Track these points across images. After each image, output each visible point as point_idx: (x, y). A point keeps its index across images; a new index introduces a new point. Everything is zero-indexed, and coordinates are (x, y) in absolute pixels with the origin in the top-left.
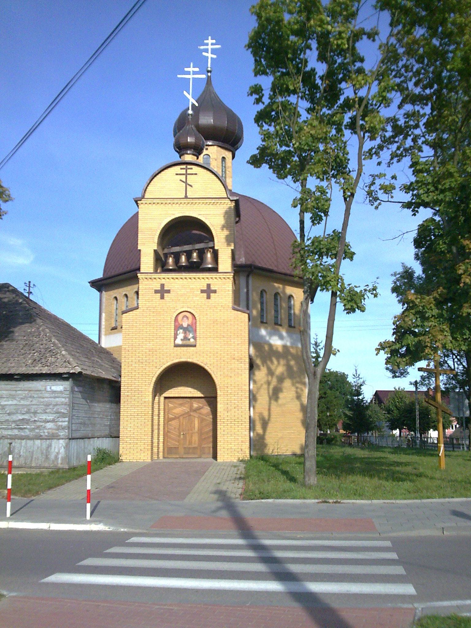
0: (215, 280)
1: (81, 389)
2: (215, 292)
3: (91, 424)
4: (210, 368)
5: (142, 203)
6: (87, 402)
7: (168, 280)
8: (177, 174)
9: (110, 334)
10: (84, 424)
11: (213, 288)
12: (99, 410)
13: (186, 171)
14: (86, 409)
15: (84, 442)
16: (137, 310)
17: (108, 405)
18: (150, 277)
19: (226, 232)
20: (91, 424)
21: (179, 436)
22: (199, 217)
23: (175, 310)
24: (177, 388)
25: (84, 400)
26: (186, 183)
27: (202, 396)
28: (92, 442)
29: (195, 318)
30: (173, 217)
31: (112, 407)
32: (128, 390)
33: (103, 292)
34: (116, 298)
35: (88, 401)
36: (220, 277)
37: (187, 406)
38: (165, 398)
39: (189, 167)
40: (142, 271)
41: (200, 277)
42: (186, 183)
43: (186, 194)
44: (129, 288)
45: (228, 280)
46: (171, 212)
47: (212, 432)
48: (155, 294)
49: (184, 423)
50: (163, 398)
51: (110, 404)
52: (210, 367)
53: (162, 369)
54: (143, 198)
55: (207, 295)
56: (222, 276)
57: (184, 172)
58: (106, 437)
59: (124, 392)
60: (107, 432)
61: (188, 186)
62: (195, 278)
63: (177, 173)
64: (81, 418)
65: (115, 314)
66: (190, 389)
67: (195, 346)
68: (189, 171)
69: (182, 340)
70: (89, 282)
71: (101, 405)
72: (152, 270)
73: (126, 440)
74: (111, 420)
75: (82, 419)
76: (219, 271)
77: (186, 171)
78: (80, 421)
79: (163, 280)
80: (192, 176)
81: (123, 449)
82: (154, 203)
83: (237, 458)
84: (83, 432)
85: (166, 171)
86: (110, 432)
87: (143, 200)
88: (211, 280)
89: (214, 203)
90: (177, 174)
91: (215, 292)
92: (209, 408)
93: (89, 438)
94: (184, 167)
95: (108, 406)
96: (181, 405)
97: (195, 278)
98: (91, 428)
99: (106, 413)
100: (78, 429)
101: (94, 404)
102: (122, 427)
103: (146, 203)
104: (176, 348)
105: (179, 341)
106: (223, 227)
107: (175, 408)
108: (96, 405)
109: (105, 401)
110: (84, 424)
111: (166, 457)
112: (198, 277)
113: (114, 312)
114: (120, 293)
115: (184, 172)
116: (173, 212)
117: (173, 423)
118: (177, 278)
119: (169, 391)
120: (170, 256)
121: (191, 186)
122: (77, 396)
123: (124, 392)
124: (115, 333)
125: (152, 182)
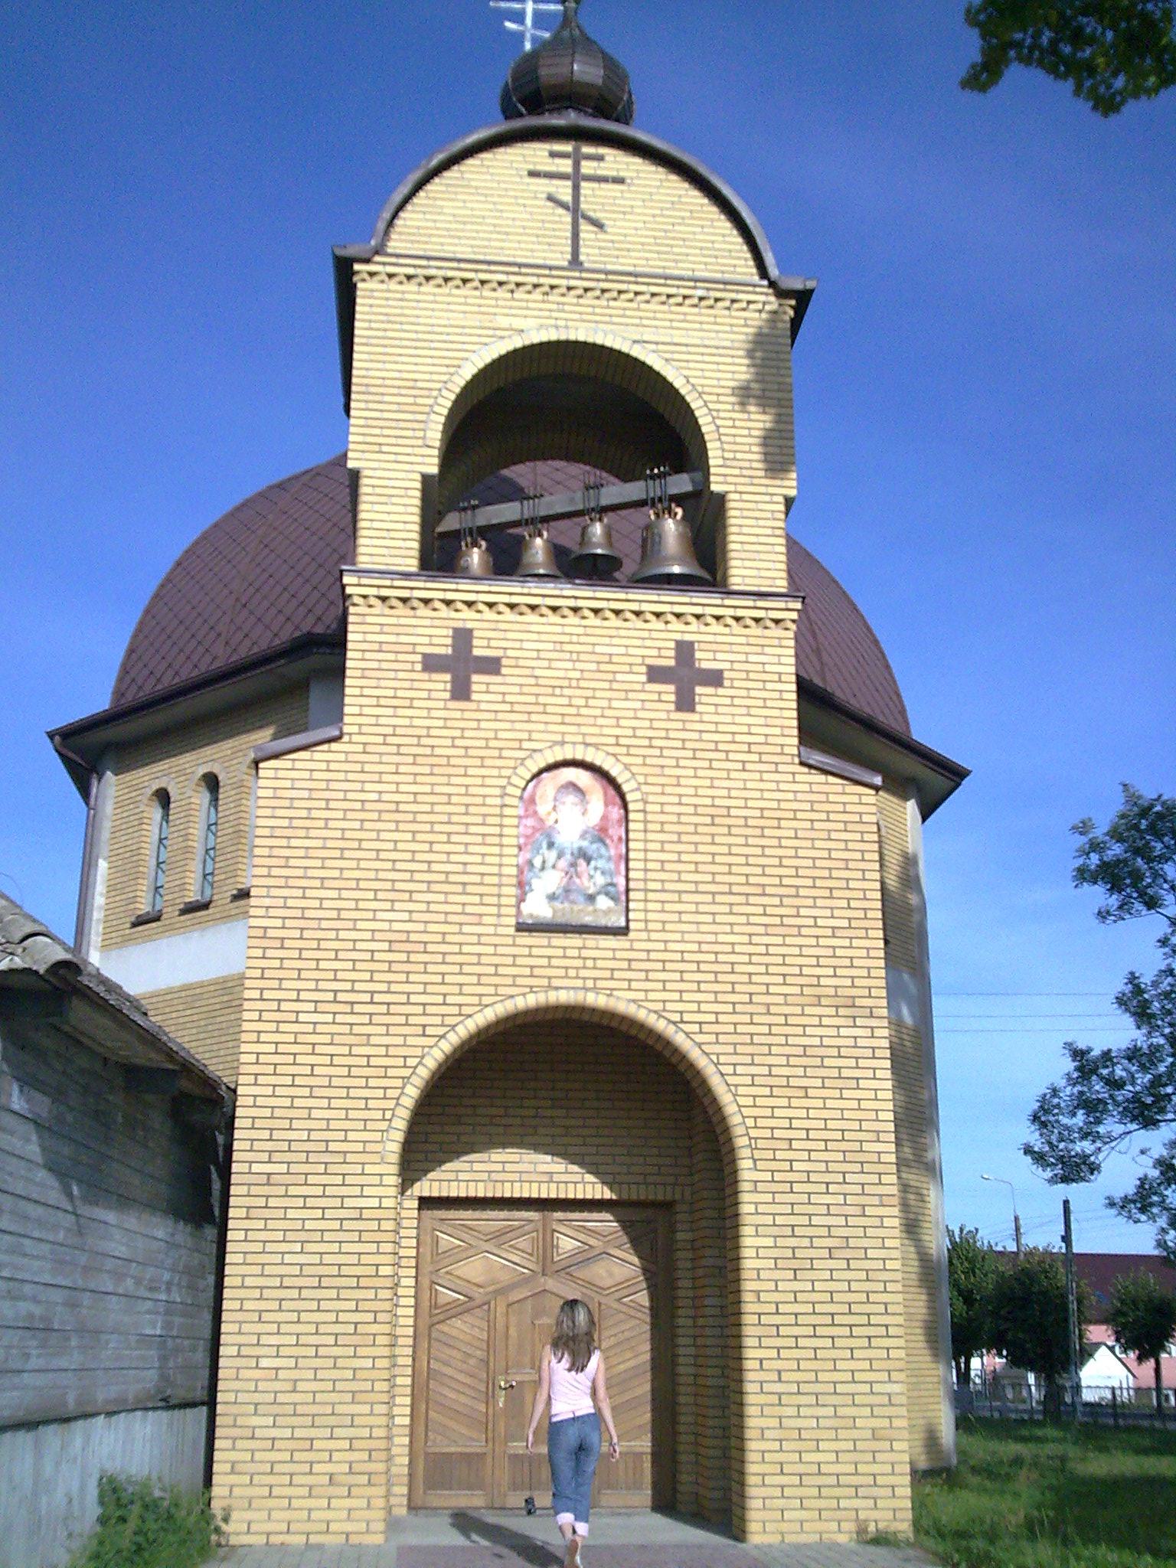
0: (716, 627)
1: (43, 1105)
2: (715, 679)
3: (82, 1330)
4: (699, 1045)
5: (372, 274)
6: (70, 1196)
7: (488, 614)
8: (533, 174)
9: (125, 942)
10: (40, 1329)
11: (705, 660)
12: (122, 1251)
13: (577, 165)
14: (61, 1236)
15: (37, 1444)
16: (334, 746)
17: (161, 1229)
18: (405, 594)
19: (759, 421)
20: (82, 1330)
21: (489, 1398)
22: (636, 352)
23: (522, 754)
24: (483, 1156)
25: (52, 1181)
26: (575, 209)
27: (608, 1194)
28: (78, 1442)
29: (622, 796)
30: (517, 343)
31: (179, 1238)
32: (269, 1146)
33: (109, 773)
34: (163, 798)
35: (75, 1190)
36: (740, 613)
37: (523, 1243)
38: (425, 1203)
39: (587, 149)
40: (363, 561)
41: (645, 607)
42: (575, 209)
43: (575, 252)
44: (227, 747)
45: (776, 632)
46: (504, 322)
47: (648, 1376)
48: (425, 676)
49: (513, 1332)
50: (415, 1204)
51: (170, 1222)
52: (699, 1038)
53: (454, 1039)
54: (377, 253)
55: (678, 693)
56: (747, 608)
57: (565, 166)
58: (143, 1406)
59: (250, 1156)
60: (150, 1378)
61: (584, 226)
62: (617, 612)
63: (531, 167)
64: (28, 1289)
65: (154, 862)
66: (547, 1163)
67: (624, 931)
68: (587, 167)
69: (552, 897)
70: (51, 735)
71: (132, 1221)
72: (412, 564)
73: (255, 1421)
74: (170, 1308)
75: (35, 1300)
76: (736, 582)
77: (577, 165)
78: (24, 1307)
79: (467, 613)
80: (603, 185)
81: (233, 1472)
82: (428, 278)
83: (850, 1526)
84: (40, 1380)
85: (486, 156)
86: (164, 1378)
87: (377, 258)
88: (695, 625)
89: (701, 299)
90: (533, 174)
91: (715, 679)
92: (636, 1260)
93: (67, 1420)
94: (567, 147)
95: (160, 1233)
96: (499, 1237)
97: (617, 612)
98: (75, 1360)
99: (150, 1272)
100: (13, 1365)
101: (100, 1213)
102: (234, 1351)
103: (391, 276)
104: (526, 939)
105: (537, 907)
106: (744, 395)
107: (467, 1252)
108: (111, 1217)
109: (150, 1206)
110: (40, 1329)
111: (419, 1503)
112: (635, 607)
113: (149, 850)
114: (182, 772)
115: (565, 166)
116: (518, 323)
117: (458, 1327)
118: (533, 608)
119: (448, 1166)
120: (475, 544)
121: (598, 225)
122: (15, 1144)
123: (250, 1156)
124: (149, 938)
125: (422, 194)
